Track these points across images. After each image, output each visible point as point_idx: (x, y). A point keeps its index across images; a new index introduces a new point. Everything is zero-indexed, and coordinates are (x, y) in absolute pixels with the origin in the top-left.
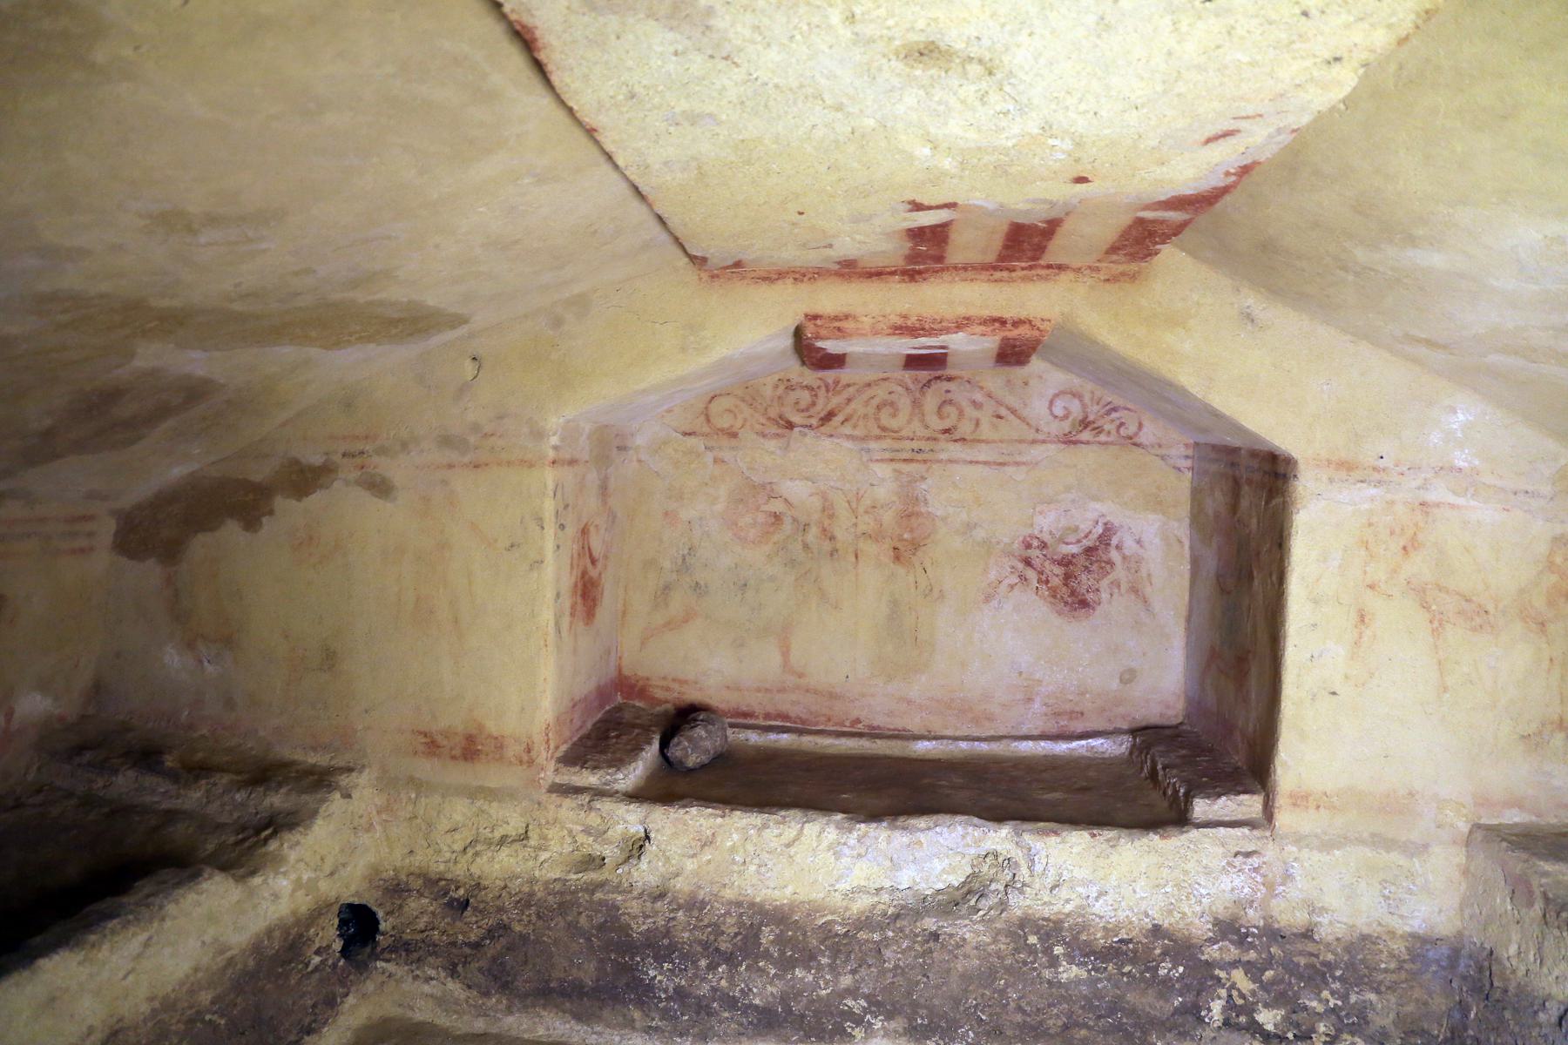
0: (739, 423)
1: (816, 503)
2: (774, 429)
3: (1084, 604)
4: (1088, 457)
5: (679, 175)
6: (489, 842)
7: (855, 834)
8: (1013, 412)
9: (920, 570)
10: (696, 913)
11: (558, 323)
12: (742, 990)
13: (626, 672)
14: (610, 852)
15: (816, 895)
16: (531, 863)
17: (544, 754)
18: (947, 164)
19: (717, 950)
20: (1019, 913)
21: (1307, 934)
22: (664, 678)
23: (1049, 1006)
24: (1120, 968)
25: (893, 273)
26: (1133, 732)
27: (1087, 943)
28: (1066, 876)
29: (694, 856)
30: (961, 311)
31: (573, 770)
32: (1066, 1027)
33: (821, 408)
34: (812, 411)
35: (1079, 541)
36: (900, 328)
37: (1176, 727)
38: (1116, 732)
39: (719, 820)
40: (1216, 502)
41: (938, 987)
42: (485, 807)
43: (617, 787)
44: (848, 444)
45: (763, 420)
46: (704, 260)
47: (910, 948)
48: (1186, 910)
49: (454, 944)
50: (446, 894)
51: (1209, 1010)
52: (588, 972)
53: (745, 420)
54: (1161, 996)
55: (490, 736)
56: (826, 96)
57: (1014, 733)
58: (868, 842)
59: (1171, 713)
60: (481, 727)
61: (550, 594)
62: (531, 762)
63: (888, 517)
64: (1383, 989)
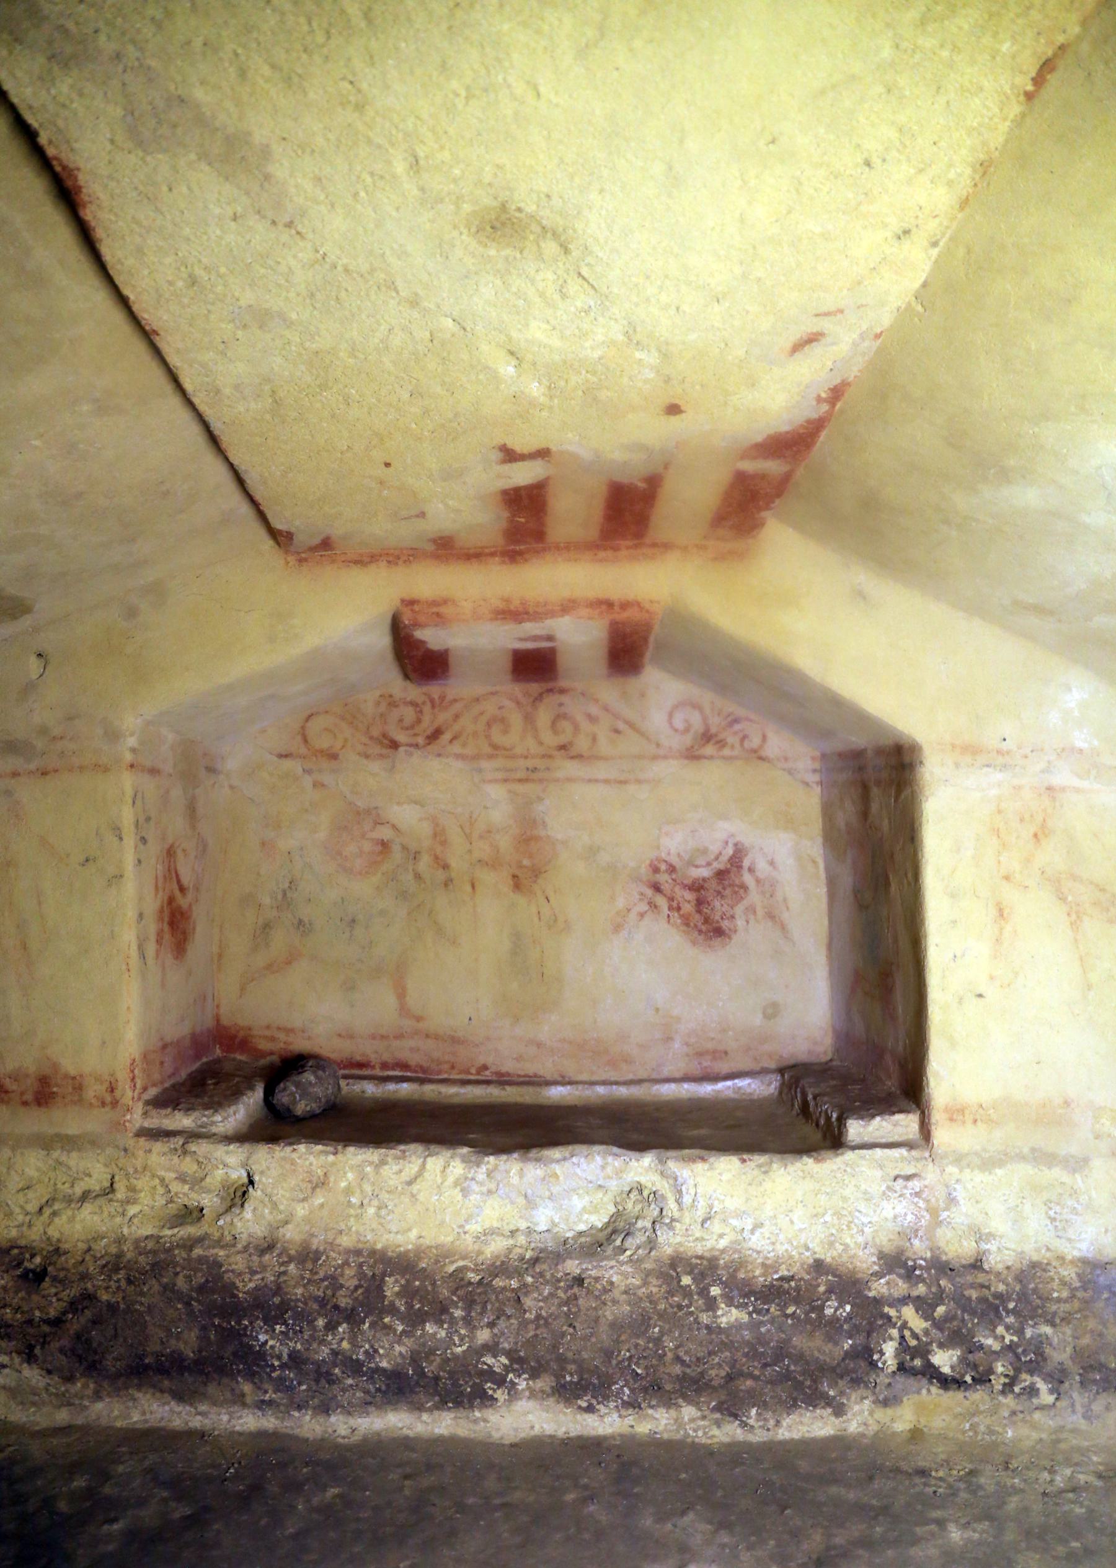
0: (339, 744)
1: (426, 829)
2: (377, 750)
3: (719, 932)
4: (713, 774)
5: (253, 405)
6: (69, 1200)
7: (484, 1168)
8: (631, 725)
9: (542, 900)
10: (309, 1265)
11: (132, 613)
12: (366, 1352)
13: (225, 1022)
14: (209, 1201)
15: (446, 1239)
16: (118, 1220)
17: (129, 1093)
18: (535, 389)
19: (336, 1307)
20: (669, 1251)
21: (977, 1265)
22: (268, 1027)
23: (710, 1353)
24: (783, 1308)
25: (493, 554)
26: (781, 1071)
27: (747, 1282)
28: (717, 1207)
29: (304, 1200)
30: (566, 593)
31: (164, 1112)
32: (730, 1378)
33: (427, 724)
34: (417, 730)
35: (709, 864)
36: (503, 612)
37: (826, 1063)
38: (764, 1071)
39: (331, 1158)
40: (847, 813)
41: (585, 1338)
42: (64, 1158)
43: (214, 1129)
44: (459, 764)
45: (365, 740)
46: (289, 536)
47: (551, 1295)
48: (848, 1241)
49: (30, 1322)
50: (19, 1265)
51: (882, 1353)
52: (188, 1342)
53: (346, 740)
54: (829, 1338)
55: (66, 1076)
56: (400, 285)
57: (654, 1076)
58: (498, 1176)
59: (820, 1049)
60: (55, 1067)
61: (131, 914)
62: (115, 1103)
63: (505, 843)
64: (1058, 1321)
